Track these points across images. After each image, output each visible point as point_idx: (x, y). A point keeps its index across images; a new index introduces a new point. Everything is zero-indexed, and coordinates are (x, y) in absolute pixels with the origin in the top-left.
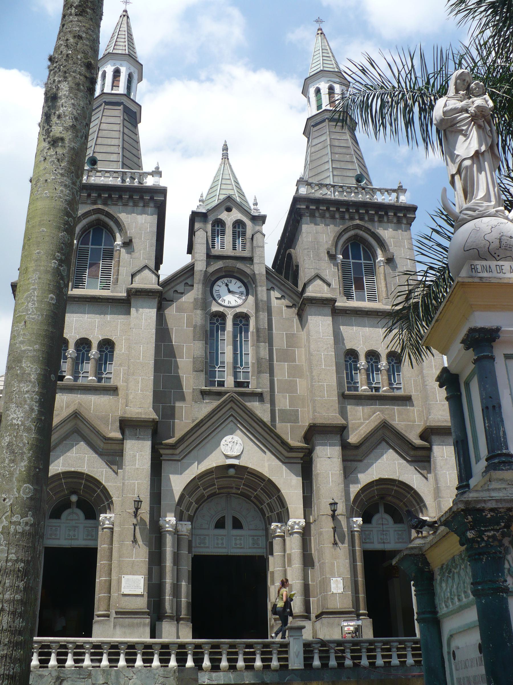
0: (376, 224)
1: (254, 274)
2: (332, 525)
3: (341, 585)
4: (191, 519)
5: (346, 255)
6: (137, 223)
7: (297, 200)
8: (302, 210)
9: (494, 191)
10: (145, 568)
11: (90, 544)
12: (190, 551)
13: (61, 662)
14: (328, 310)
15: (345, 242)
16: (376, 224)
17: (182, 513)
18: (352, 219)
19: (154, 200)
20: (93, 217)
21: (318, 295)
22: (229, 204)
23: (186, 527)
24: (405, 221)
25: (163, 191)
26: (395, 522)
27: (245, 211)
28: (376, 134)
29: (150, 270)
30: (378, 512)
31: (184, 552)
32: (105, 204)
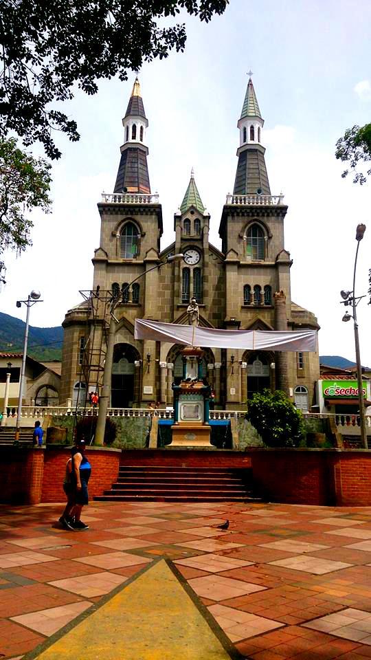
0: (265, 218)
1: (203, 249)
2: (161, 238)
3: (234, 391)
4: (173, 362)
5: (248, 235)
6: (148, 225)
7: (226, 208)
8: (228, 212)
9: (258, 509)
10: (153, 383)
11: (114, 364)
12: (173, 376)
13: (121, 415)
14: (236, 267)
15: (250, 228)
16: (265, 218)
17: (169, 359)
18: (253, 216)
19: (156, 211)
20: (127, 221)
21: (232, 260)
22: (192, 210)
23: (171, 365)
24: (281, 215)
25: (159, 207)
26: (263, 364)
27: (201, 214)
28: (276, 536)
29: (154, 250)
30: (256, 359)
31: (171, 376)
32: (132, 214)
